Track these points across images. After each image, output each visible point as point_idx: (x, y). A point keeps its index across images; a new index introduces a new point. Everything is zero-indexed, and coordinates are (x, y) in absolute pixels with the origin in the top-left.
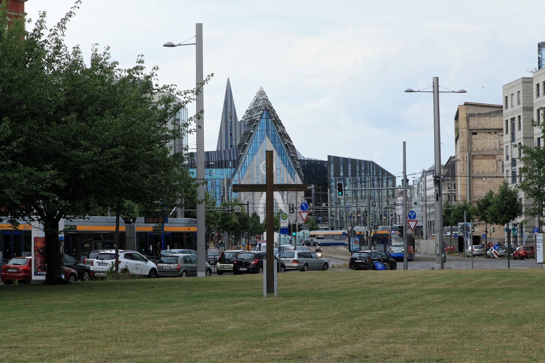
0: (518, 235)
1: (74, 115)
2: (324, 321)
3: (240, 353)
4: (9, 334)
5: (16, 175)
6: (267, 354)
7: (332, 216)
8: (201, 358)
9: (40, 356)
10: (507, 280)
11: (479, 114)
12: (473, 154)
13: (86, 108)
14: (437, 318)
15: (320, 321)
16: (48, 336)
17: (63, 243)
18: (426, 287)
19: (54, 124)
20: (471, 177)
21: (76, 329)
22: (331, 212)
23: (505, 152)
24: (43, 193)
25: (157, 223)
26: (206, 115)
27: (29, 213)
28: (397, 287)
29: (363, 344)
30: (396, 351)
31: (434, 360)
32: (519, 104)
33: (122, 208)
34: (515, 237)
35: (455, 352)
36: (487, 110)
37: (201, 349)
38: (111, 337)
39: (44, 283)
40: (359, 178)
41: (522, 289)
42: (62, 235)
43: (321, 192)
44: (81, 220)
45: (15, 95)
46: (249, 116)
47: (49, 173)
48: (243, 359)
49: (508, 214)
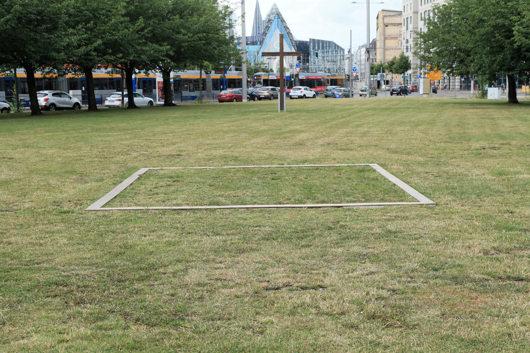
0: (409, 80)
1: (178, 16)
2: (312, 125)
3: (269, 142)
4: (145, 133)
5: (147, 48)
6: (283, 142)
7: (311, 70)
8: (248, 145)
9: (162, 144)
10: (405, 103)
11: (389, 16)
12: (385, 37)
13: (183, 12)
14: (371, 123)
15: (310, 125)
16: (166, 133)
17: (173, 85)
18: (363, 107)
19: (167, 20)
20: (385, 49)
21: (181, 130)
22: (311, 68)
23: (403, 36)
24: (162, 58)
25: (222, 73)
26: (246, 15)
27: (154, 68)
28: (348, 107)
29: (334, 137)
30: (351, 141)
31: (373, 146)
32: (411, 10)
33: (203, 66)
34: (407, 81)
35: (384, 141)
36: (394, 14)
37: (248, 140)
38: (199, 133)
39: (164, 105)
40: (325, 50)
41: (414, 108)
42: (172, 80)
43: (306, 58)
44: (182, 72)
45: (146, 4)
46: (268, 17)
47: (166, 47)
48: (270, 145)
49: (404, 68)
